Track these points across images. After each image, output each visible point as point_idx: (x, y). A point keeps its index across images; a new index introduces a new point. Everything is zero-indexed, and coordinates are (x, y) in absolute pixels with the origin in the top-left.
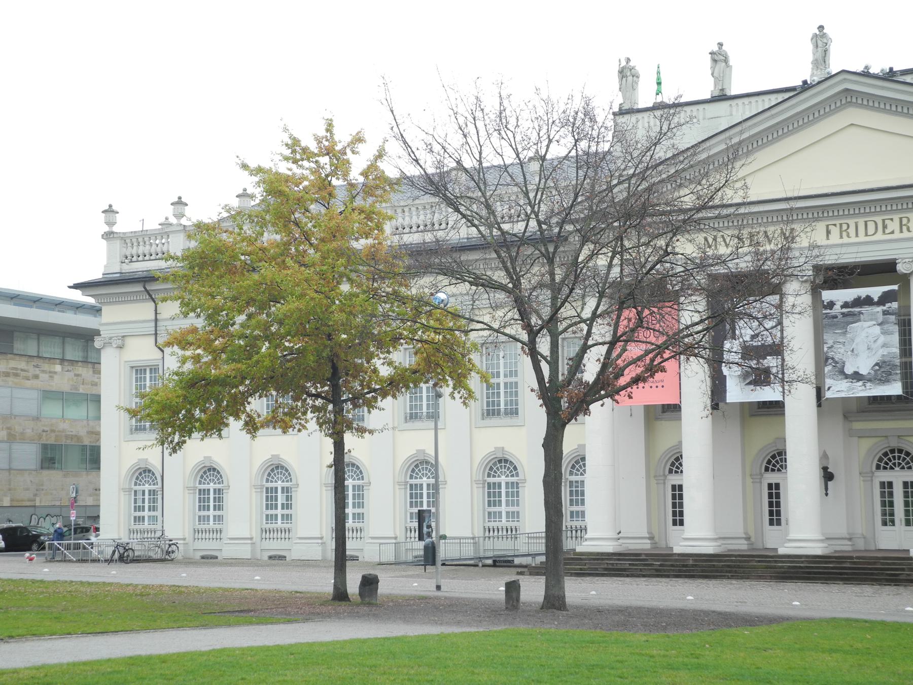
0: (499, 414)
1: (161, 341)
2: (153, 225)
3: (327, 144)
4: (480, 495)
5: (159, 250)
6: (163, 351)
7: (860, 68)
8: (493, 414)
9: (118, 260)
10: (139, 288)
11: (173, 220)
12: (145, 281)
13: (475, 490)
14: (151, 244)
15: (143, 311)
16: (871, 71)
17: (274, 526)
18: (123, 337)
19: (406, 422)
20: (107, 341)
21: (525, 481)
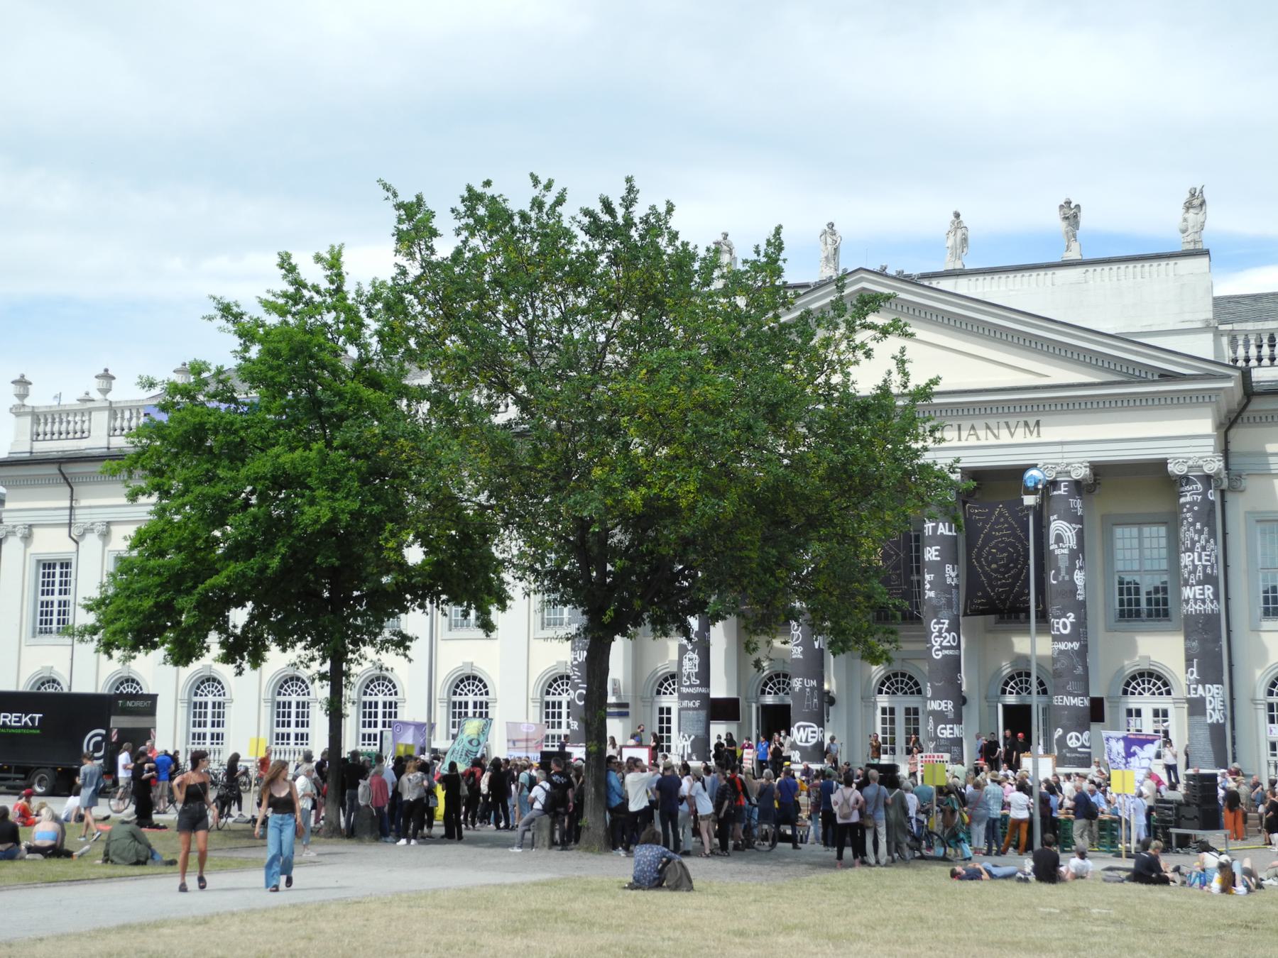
0: (561, 624)
1: (75, 533)
2: (70, 400)
3: (379, 305)
4: (267, 712)
5: (78, 427)
6: (77, 543)
7: (877, 268)
8: (1130, 615)
9: (105, 432)
10: (53, 470)
11: (96, 395)
12: (61, 463)
13: (179, 710)
14: (68, 422)
15: (56, 501)
16: (888, 271)
18: (108, 523)
19: (34, 636)
20: (10, 529)
21: (495, 701)
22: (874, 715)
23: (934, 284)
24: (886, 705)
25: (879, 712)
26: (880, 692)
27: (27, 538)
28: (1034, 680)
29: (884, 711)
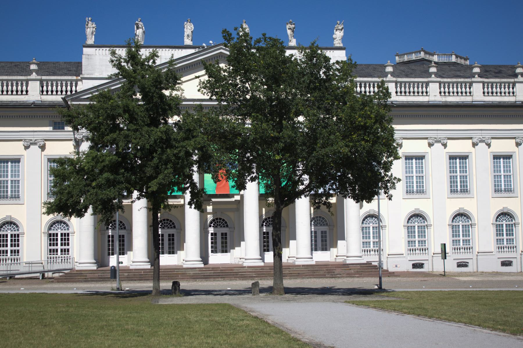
4: (45, 240)
17: (55, 256)
22: (208, 236)
23: (197, 50)
24: (213, 232)
25: (210, 235)
26: (210, 226)
27: (43, 148)
28: (117, 223)
29: (212, 234)
